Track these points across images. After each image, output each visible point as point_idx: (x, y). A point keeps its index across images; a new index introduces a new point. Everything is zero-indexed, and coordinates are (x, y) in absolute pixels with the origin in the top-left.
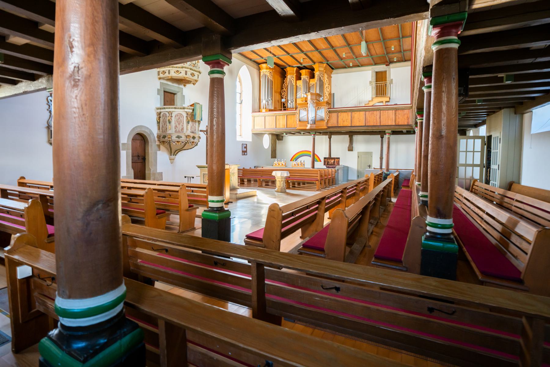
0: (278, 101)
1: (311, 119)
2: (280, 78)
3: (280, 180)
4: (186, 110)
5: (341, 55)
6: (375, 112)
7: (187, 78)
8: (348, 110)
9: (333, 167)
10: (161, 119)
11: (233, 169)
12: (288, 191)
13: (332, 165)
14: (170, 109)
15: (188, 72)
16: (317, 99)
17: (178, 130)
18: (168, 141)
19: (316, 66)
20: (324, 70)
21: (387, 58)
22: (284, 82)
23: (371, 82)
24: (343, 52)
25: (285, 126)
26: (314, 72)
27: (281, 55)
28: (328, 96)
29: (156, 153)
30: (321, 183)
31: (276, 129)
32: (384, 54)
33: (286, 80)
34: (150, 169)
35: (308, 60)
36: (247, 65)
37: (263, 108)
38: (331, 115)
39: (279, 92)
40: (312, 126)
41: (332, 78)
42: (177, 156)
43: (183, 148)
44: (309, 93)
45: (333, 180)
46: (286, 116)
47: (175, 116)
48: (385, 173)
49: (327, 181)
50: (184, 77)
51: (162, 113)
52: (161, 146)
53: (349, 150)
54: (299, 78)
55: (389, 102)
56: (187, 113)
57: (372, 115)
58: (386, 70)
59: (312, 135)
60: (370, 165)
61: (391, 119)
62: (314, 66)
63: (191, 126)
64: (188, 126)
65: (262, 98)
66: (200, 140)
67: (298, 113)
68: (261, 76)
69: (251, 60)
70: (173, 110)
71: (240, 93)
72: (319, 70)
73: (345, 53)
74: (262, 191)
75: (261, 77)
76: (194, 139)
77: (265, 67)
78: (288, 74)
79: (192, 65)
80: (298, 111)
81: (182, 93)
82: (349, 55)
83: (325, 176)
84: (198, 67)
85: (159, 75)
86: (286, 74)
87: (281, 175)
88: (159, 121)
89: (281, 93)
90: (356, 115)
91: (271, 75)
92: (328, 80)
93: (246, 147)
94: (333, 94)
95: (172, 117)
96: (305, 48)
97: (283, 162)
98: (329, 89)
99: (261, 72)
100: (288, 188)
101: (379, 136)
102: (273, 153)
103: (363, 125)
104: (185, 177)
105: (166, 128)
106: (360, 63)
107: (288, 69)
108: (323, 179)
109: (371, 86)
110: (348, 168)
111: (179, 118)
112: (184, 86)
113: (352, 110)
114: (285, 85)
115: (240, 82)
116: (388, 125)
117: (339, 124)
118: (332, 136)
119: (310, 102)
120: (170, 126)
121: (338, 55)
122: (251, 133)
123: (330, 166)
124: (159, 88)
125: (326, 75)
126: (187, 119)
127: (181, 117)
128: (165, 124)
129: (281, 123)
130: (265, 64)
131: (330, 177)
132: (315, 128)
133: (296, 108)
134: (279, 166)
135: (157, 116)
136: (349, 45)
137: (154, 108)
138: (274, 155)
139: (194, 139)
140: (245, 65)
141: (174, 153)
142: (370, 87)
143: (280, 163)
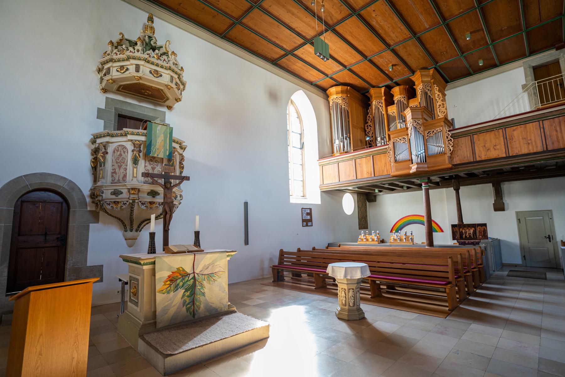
0: (361, 141)
2: (361, 108)
3: (345, 287)
8: (495, 126)
9: (473, 244)
11: (209, 265)
13: (470, 238)
15: (141, 67)
17: (117, 179)
20: (431, 80)
25: (371, 175)
31: (357, 181)
35: (401, 67)
38: (457, 142)
40: (421, 166)
41: (446, 96)
46: (371, 157)
47: (114, 152)
53: (496, 210)
62: (413, 78)
67: (392, 149)
68: (330, 105)
69: (311, 83)
71: (300, 134)
72: (422, 82)
78: (373, 99)
83: (464, 266)
86: (370, 101)
89: (365, 129)
90: (517, 133)
91: (344, 102)
92: (440, 94)
93: (310, 214)
96: (392, 35)
97: (373, 235)
99: (330, 100)
103: (540, 149)
104: (120, 280)
107: (373, 91)
110: (499, 241)
111: (121, 155)
113: (505, 124)
114: (369, 116)
115: (299, 117)
117: (477, 155)
118: (461, 187)
119: (411, 124)
122: (319, 191)
123: (467, 241)
125: (435, 88)
127: (124, 152)
134: (368, 243)
141: (139, 227)
142: (526, 96)
143: (369, 237)
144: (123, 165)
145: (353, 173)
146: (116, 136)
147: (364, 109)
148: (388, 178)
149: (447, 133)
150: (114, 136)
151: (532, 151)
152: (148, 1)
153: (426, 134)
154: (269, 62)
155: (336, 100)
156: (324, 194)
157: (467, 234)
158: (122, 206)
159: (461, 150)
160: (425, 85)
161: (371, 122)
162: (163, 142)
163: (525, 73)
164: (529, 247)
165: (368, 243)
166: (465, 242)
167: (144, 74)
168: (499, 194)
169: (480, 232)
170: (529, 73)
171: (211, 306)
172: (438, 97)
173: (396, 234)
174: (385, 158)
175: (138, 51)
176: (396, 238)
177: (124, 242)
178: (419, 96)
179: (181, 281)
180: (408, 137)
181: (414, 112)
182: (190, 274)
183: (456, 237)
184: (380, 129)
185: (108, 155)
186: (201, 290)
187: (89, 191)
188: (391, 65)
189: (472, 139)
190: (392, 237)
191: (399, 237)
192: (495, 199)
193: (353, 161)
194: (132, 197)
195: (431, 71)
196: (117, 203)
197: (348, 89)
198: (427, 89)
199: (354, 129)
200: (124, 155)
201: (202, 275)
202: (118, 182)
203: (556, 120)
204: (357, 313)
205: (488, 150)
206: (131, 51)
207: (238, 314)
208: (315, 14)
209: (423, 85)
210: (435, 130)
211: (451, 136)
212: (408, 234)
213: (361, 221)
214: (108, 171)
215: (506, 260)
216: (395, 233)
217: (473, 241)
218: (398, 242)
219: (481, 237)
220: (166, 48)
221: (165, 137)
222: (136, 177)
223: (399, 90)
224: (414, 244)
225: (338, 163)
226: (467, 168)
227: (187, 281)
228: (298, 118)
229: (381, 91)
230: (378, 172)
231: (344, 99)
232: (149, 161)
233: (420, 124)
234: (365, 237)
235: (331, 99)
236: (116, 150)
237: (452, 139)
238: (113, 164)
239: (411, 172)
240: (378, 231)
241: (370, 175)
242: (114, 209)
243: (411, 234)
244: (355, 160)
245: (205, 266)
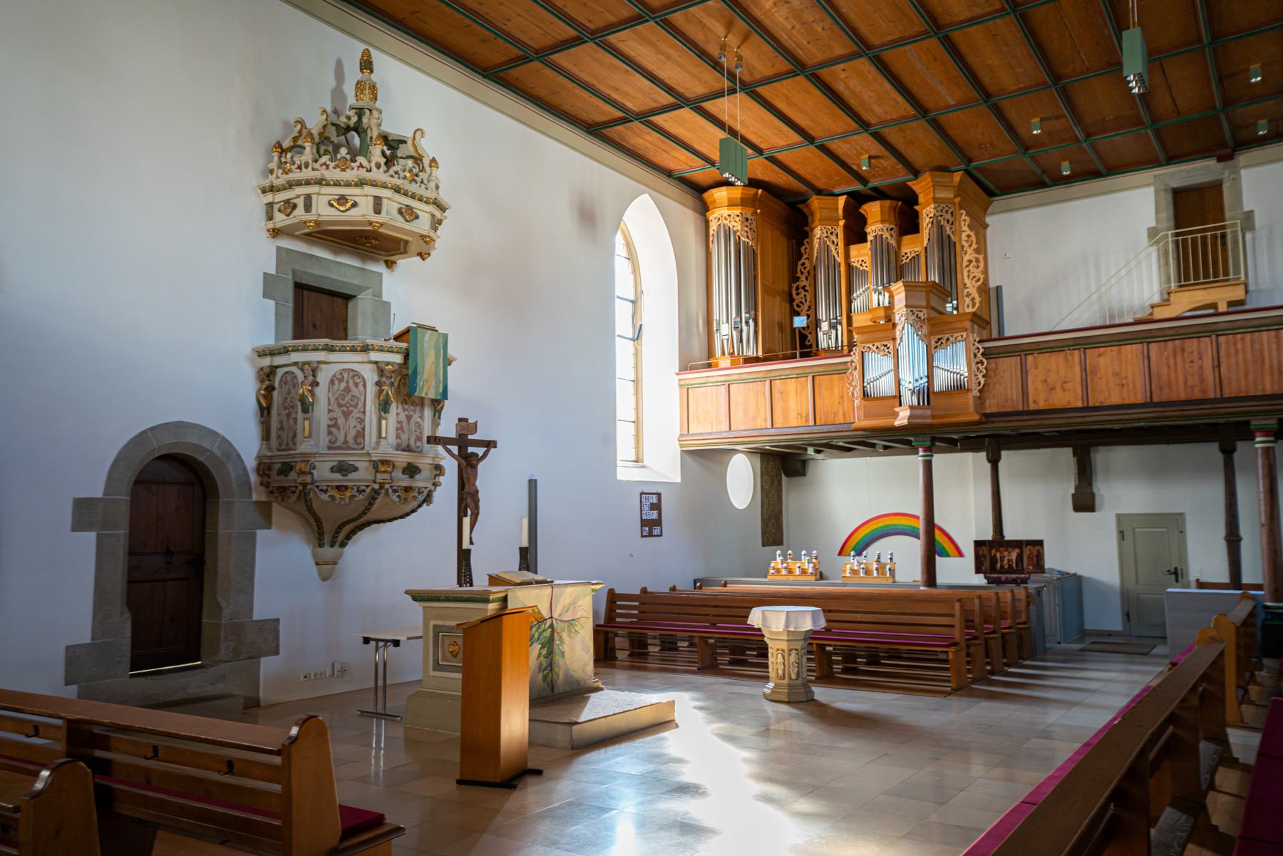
0: (781, 326)
1: (911, 386)
3: (784, 646)
4: (374, 356)
5: (1022, 131)
6: (1192, 345)
7: (382, 225)
8: (1067, 343)
9: (1014, 581)
10: (275, 394)
12: (822, 693)
13: (1011, 570)
14: (304, 354)
15: (385, 202)
16: (932, 304)
17: (341, 439)
18: (300, 488)
19: (922, 187)
20: (956, 196)
21: (1225, 125)
22: (800, 256)
23: (1152, 233)
24: (1035, 116)
25: (807, 421)
26: (916, 207)
27: (783, 147)
28: (976, 295)
29: (252, 540)
30: (968, 655)
32: (1214, 107)
33: (806, 245)
34: (221, 608)
35: (889, 162)
36: (652, 192)
37: (723, 354)
39: (783, 292)
40: (919, 412)
41: (988, 230)
43: (364, 513)
44: (900, 284)
45: (1020, 637)
46: (810, 378)
47: (332, 382)
48: (1265, 607)
49: (996, 646)
50: (370, 223)
51: (280, 372)
52: (276, 508)
53: (1079, 507)
54: (856, 233)
55: (1241, 302)
56: (378, 368)
57: (1179, 359)
58: (1219, 177)
59: (920, 449)
60: (1176, 568)
61: (1271, 366)
62: (916, 186)
63: (400, 422)
64: (384, 422)
65: (716, 316)
66: (441, 479)
68: (711, 232)
69: (669, 174)
70: (321, 356)
72: (935, 200)
73: (1041, 120)
74: (708, 698)
75: (711, 239)
76: (412, 477)
77: (726, 200)
78: (817, 222)
79: (402, 174)
80: (855, 357)
81: (378, 294)
82: (1056, 125)
83: (986, 622)
84: (432, 185)
85: (270, 218)
86: (807, 225)
87: (787, 625)
88: (265, 405)
89: (791, 295)
90: (1105, 360)
92: (972, 234)
93: (657, 507)
94: (998, 289)
95: (315, 384)
96: (876, 108)
97: (805, 559)
98: (978, 267)
99: (711, 218)
100: (827, 678)
101: (1214, 447)
102: (770, 524)
104: (367, 641)
105: (291, 434)
106: (1102, 160)
108: (976, 638)
109: (1155, 248)
110: (1078, 579)
111: (348, 390)
112: (388, 267)
114: (803, 264)
115: (632, 257)
116: (1260, 393)
118: (1004, 453)
119: (903, 319)
120: (307, 423)
121: (1011, 129)
122: (678, 449)
123: (1003, 577)
125: (963, 217)
126: (381, 392)
127: (356, 385)
128: (288, 415)
129: (793, 404)
130: (724, 188)
131: (1008, 623)
132: (930, 421)
133: (851, 345)
134: (791, 578)
135: (259, 384)
136: (1057, 78)
137: (247, 347)
138: (773, 532)
139: (412, 477)
140: (646, 195)
142: (1153, 253)
144: (355, 411)
145: (765, 412)
146: (340, 351)
147: (790, 242)
148: (846, 431)
149: (975, 347)
150: (335, 351)
151: (1127, 402)
152: (345, 3)
153: (933, 342)
154: (581, 129)
155: (727, 222)
156: (688, 459)
157: (1006, 562)
158: (355, 496)
159: (1000, 384)
160: (941, 208)
161: (807, 279)
162: (434, 365)
163: (1157, 202)
164: (1138, 594)
165: (791, 578)
166: (999, 578)
167: (391, 219)
168: (1085, 474)
169: (1030, 558)
170: (1163, 204)
171: (572, 675)
172: (967, 241)
173: (857, 558)
174: (841, 386)
176: (856, 568)
177: (314, 569)
178: (925, 231)
179: (537, 630)
180: (894, 346)
181: (911, 291)
182: (546, 619)
183: (983, 568)
184: (828, 297)
186: (560, 647)
187: (255, 460)
188: (867, 156)
189: (1024, 364)
190: (848, 566)
191: (862, 566)
192: (1077, 483)
193: (765, 385)
194: (380, 477)
195: (957, 177)
196: (344, 488)
197: (757, 194)
198: (944, 219)
199: (766, 296)
200: (356, 389)
201: (562, 621)
202: (344, 446)
203: (1170, 344)
204: (803, 690)
205: (1052, 389)
206: (361, 164)
207: (606, 692)
208: (722, 68)
209: (935, 208)
211: (983, 354)
212: (882, 560)
213: (767, 525)
214: (319, 422)
215: (1093, 621)
216: (854, 556)
217: (1014, 576)
218: (862, 577)
219: (1031, 568)
221: (437, 356)
222: (385, 438)
223: (879, 209)
224: (894, 582)
225: (729, 385)
226: (1010, 424)
227: (544, 631)
228: (629, 259)
229: (837, 204)
230: (823, 416)
231: (747, 220)
232: (402, 403)
233: (922, 318)
234: (785, 565)
235: (715, 215)
236: (338, 379)
237: (984, 360)
238: (330, 408)
239: (897, 423)
240: (815, 552)
241: (804, 420)
242: (337, 502)
243: (891, 559)
244: (771, 381)
245: (564, 607)
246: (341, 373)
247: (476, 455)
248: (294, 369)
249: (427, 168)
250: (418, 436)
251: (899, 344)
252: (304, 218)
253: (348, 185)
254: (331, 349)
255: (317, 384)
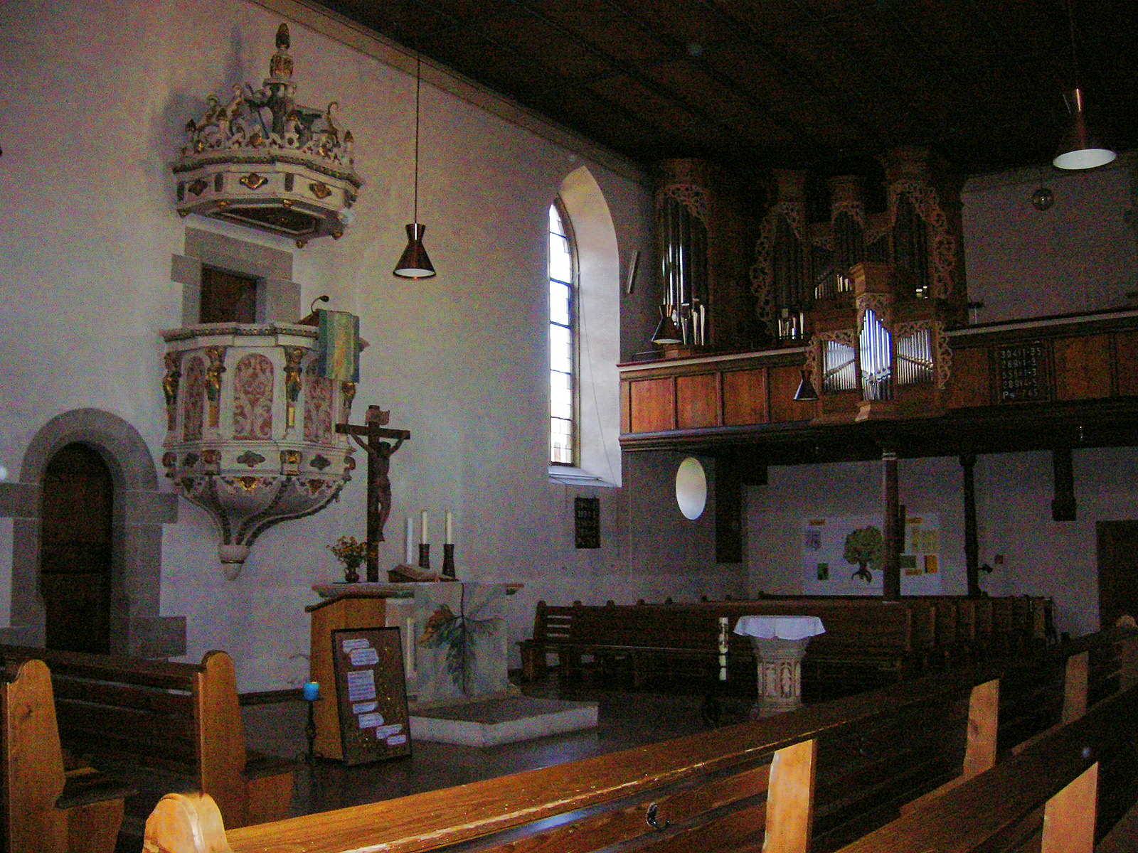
4: (285, 340)
15: (296, 178)
42: (254, 547)
47: (239, 368)
63: (308, 411)
64: (291, 410)
66: (352, 473)
70: (228, 340)
114: (762, 243)
119: (864, 304)
124: (181, 252)
126: (289, 377)
127: (263, 371)
161: (765, 260)
168: (1064, 480)
175: (291, 142)
182: (456, 618)
185: (226, 373)
210: (916, 324)
220: (329, 120)
246: (248, 359)
247: (389, 445)
248: (201, 354)
249: (342, 143)
250: (327, 426)
251: (861, 333)
252: (215, 198)
253: (260, 162)
254: (236, 333)
255: (224, 370)
